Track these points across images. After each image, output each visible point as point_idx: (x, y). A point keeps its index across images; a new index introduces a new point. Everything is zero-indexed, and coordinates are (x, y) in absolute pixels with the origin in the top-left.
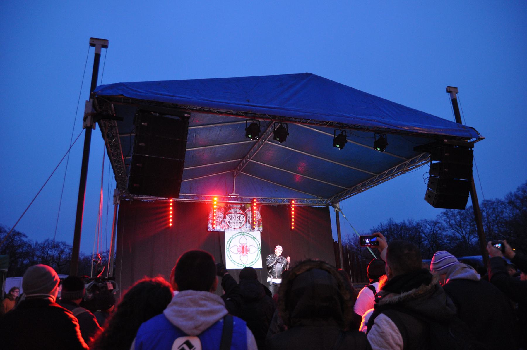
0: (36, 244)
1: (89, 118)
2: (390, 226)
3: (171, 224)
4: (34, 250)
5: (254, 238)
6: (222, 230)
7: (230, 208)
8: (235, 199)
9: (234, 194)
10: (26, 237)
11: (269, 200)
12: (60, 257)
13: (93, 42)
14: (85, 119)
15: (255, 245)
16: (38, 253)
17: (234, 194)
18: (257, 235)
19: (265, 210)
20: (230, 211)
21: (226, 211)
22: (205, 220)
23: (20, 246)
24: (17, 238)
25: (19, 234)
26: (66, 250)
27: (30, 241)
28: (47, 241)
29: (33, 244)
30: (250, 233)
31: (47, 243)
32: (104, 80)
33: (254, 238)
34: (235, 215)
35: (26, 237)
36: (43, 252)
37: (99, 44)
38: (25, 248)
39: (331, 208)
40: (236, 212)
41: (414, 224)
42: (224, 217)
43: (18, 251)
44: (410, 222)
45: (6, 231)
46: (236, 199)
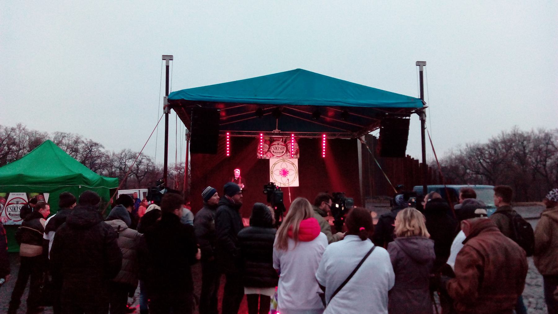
0: (114, 154)
1: (167, 108)
2: (515, 135)
3: (228, 155)
4: (112, 161)
5: (293, 164)
6: (267, 158)
7: (274, 141)
8: (276, 134)
9: (277, 130)
10: (103, 148)
11: (305, 135)
12: (138, 167)
13: (165, 57)
14: (164, 109)
15: (293, 168)
16: (116, 164)
17: (277, 130)
18: (296, 161)
19: (300, 142)
20: (274, 143)
21: (271, 142)
22: (255, 150)
23: (99, 157)
24: (94, 149)
25: (96, 144)
26: (143, 161)
27: (107, 152)
28: (124, 151)
29: (110, 154)
30: (290, 160)
31: (124, 154)
32: (174, 88)
33: (293, 164)
34: (278, 147)
35: (103, 148)
36: (121, 163)
37: (168, 58)
38: (103, 159)
39: (358, 140)
40: (278, 144)
41: (542, 135)
42: (269, 148)
43: (97, 162)
44: (540, 132)
45: (83, 142)
46: (279, 134)
